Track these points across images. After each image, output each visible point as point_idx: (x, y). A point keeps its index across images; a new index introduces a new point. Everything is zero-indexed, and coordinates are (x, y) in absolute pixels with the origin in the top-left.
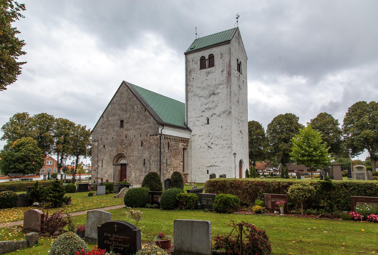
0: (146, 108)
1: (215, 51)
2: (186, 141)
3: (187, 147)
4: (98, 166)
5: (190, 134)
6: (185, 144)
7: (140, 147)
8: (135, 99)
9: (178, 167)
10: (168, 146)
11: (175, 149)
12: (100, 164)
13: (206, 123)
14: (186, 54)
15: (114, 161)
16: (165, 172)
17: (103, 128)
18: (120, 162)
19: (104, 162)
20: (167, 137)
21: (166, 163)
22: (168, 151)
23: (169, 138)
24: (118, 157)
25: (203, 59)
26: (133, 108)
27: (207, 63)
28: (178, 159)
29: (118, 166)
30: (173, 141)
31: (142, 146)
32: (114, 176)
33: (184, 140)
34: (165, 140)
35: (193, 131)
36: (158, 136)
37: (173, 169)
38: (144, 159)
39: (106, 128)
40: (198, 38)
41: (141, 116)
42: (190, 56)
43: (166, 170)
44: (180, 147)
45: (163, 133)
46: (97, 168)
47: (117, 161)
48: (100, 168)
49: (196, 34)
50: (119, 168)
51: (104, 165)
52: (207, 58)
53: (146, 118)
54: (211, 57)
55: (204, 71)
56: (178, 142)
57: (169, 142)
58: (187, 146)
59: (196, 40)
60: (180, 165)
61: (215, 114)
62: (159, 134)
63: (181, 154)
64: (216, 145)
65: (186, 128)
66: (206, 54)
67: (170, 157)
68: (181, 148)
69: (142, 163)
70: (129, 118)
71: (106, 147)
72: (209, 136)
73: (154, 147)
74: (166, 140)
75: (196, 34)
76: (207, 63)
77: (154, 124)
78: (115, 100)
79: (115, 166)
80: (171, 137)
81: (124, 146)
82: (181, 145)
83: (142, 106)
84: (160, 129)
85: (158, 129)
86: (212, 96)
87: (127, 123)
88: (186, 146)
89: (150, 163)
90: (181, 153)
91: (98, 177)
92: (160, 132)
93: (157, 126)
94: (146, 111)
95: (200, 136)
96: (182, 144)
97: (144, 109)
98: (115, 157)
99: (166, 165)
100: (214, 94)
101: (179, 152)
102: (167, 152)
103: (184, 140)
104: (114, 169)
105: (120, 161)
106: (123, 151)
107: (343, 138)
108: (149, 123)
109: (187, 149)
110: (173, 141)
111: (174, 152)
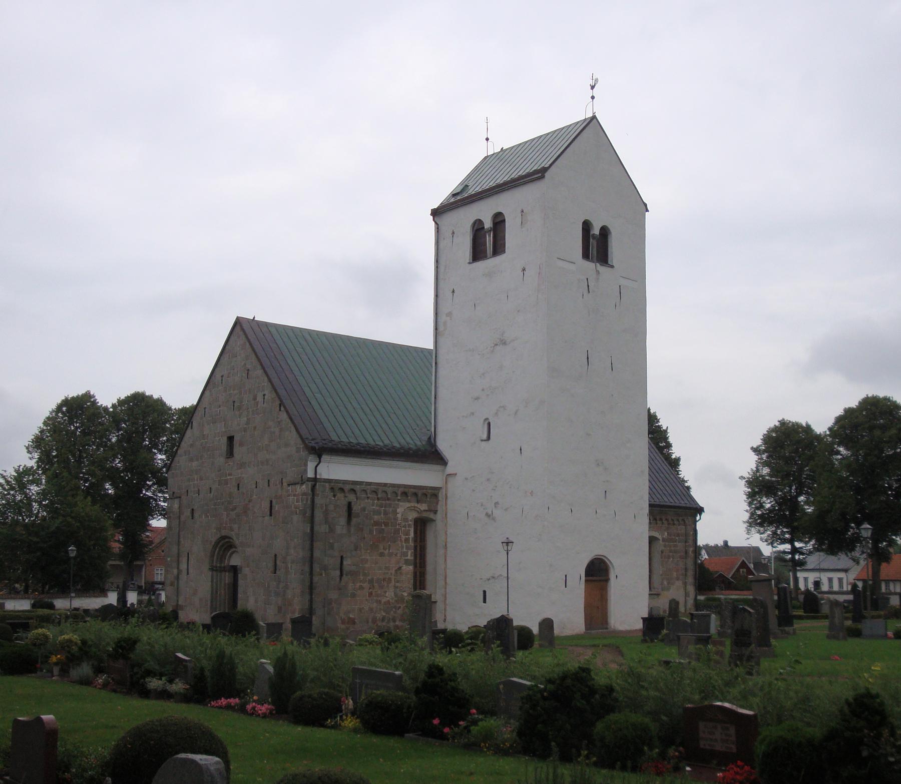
0: (281, 401)
1: (505, 203)
2: (430, 495)
3: (432, 516)
4: (179, 572)
5: (443, 471)
6: (423, 507)
7: (267, 518)
8: (260, 372)
9: (390, 579)
10: (346, 514)
11: (376, 523)
12: (183, 566)
13: (485, 436)
14: (435, 213)
15: (212, 556)
16: (333, 595)
17: (191, 460)
18: (229, 560)
19: (192, 562)
20: (338, 487)
21: (338, 566)
22: (349, 531)
23: (353, 490)
24: (222, 546)
25: (478, 229)
26: (255, 399)
27: (489, 240)
28: (390, 555)
29: (223, 574)
30: (368, 498)
31: (271, 515)
32: (212, 602)
33: (416, 494)
34: (334, 496)
35: (449, 464)
36: (304, 486)
37: (366, 585)
38: (276, 555)
39: (197, 460)
40: (490, 153)
41: (270, 423)
42: (449, 219)
43: (340, 589)
44: (399, 516)
45: (325, 476)
46: (178, 578)
47: (222, 558)
48: (183, 577)
49: (487, 139)
50: (227, 577)
51: (191, 571)
52: (488, 224)
53: (281, 430)
54: (499, 221)
55: (480, 265)
56: (388, 499)
57: (350, 504)
58: (435, 512)
59: (485, 158)
60: (401, 573)
61: (504, 407)
62: (309, 480)
63: (407, 540)
64: (506, 510)
65: (430, 455)
66: (484, 212)
67: (356, 548)
68: (406, 520)
69: (271, 565)
70: (245, 430)
71: (196, 515)
72: (488, 480)
73: (295, 518)
74: (340, 495)
75: (487, 139)
76: (489, 240)
77: (298, 451)
78: (218, 375)
79: (215, 573)
80: (357, 488)
81: (233, 514)
82: (405, 512)
83: (274, 395)
84: (311, 466)
85: (306, 465)
86: (498, 348)
87: (241, 445)
88: (430, 510)
89: (287, 568)
90: (407, 534)
91: (180, 603)
92: (310, 474)
93: (304, 453)
94: (282, 409)
95: (466, 479)
96: (408, 505)
97: (278, 402)
98: (215, 546)
99: (338, 573)
100: (504, 343)
101: (397, 531)
102: (345, 531)
103: (416, 494)
104: (212, 581)
105: (230, 556)
106: (232, 529)
107: (117, 545)
108: (287, 445)
109: (433, 520)
110: (368, 498)
111: (371, 532)
